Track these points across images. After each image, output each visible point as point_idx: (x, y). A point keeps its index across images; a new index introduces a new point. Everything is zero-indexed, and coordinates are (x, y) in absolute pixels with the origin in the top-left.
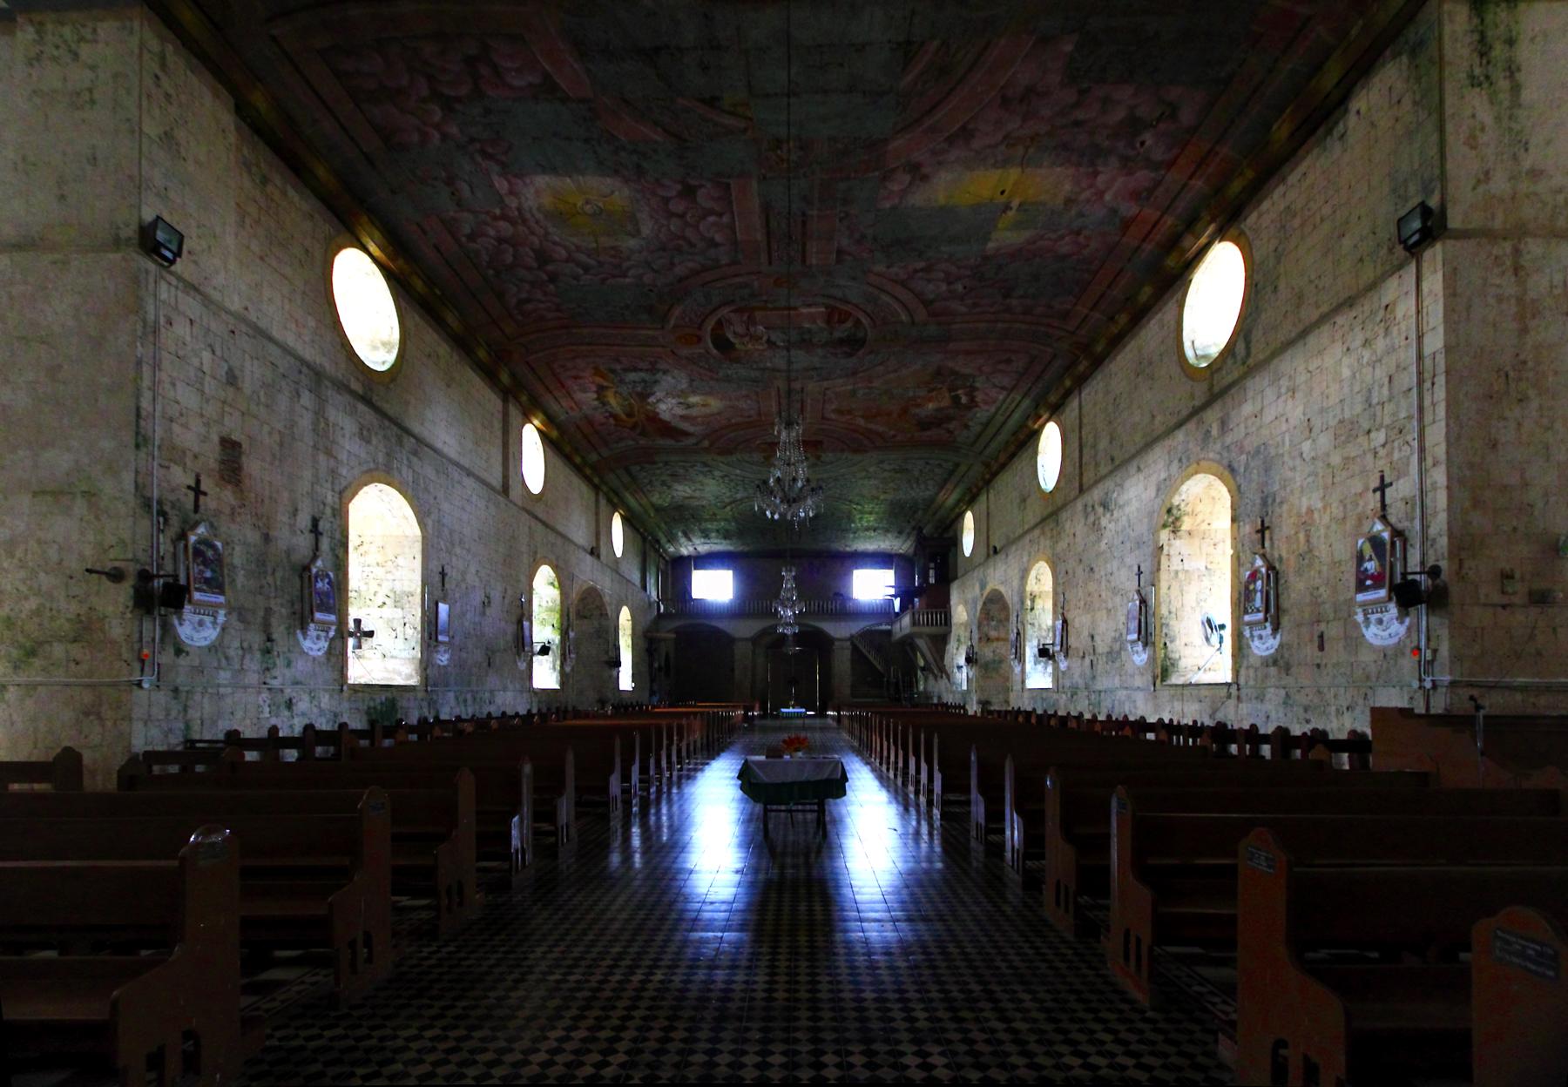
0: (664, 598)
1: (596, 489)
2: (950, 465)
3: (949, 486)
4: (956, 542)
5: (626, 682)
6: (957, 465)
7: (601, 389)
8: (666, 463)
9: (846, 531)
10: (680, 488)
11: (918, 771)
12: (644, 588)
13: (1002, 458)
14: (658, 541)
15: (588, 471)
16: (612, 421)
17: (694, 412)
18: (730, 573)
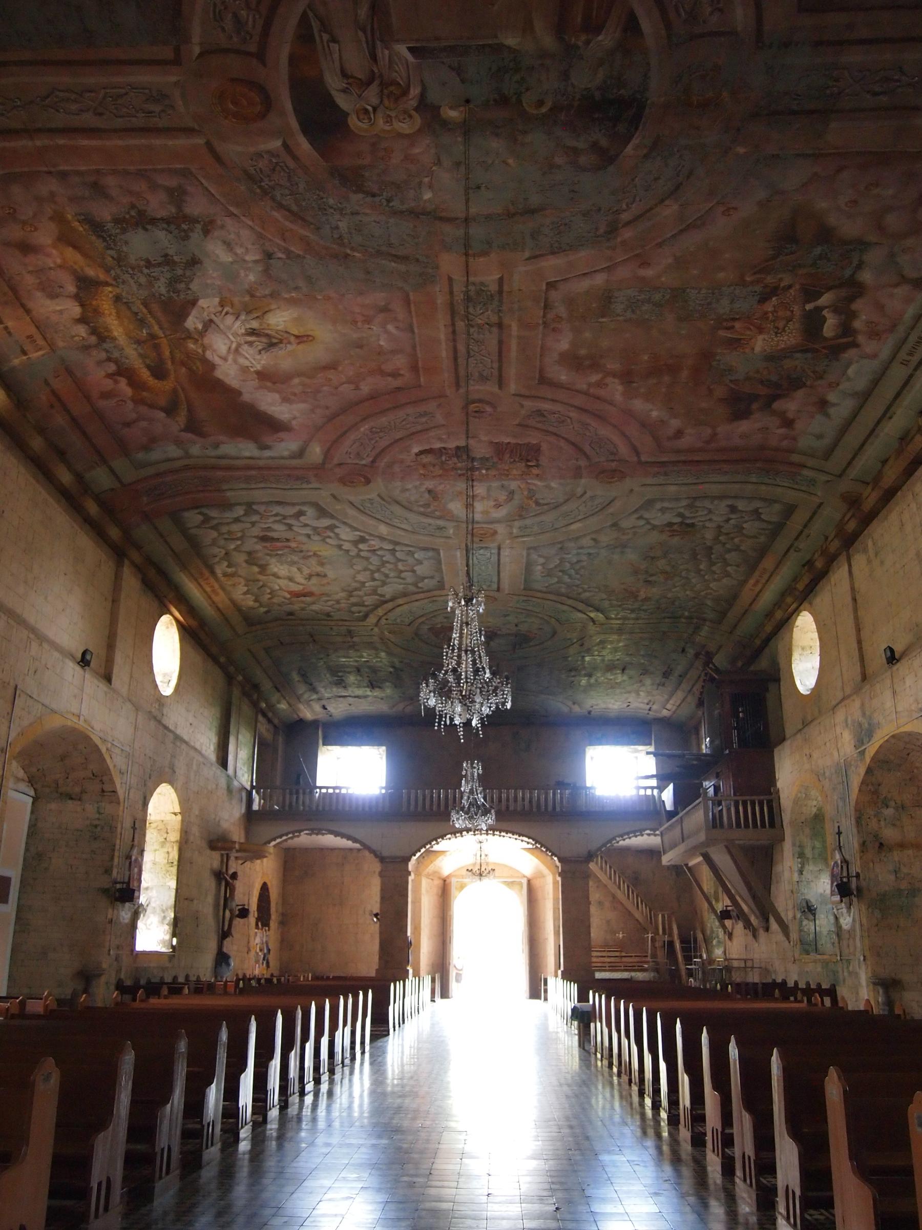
0: (263, 780)
1: (119, 553)
2: (772, 514)
3: (768, 563)
4: (777, 675)
5: (152, 935)
6: (790, 510)
7: (86, 287)
8: (250, 508)
9: (573, 670)
10: (282, 570)
11: (727, 1118)
12: (223, 762)
13: (890, 475)
14: (256, 687)
15: (92, 508)
16: (123, 385)
17: (284, 359)
18: (384, 748)
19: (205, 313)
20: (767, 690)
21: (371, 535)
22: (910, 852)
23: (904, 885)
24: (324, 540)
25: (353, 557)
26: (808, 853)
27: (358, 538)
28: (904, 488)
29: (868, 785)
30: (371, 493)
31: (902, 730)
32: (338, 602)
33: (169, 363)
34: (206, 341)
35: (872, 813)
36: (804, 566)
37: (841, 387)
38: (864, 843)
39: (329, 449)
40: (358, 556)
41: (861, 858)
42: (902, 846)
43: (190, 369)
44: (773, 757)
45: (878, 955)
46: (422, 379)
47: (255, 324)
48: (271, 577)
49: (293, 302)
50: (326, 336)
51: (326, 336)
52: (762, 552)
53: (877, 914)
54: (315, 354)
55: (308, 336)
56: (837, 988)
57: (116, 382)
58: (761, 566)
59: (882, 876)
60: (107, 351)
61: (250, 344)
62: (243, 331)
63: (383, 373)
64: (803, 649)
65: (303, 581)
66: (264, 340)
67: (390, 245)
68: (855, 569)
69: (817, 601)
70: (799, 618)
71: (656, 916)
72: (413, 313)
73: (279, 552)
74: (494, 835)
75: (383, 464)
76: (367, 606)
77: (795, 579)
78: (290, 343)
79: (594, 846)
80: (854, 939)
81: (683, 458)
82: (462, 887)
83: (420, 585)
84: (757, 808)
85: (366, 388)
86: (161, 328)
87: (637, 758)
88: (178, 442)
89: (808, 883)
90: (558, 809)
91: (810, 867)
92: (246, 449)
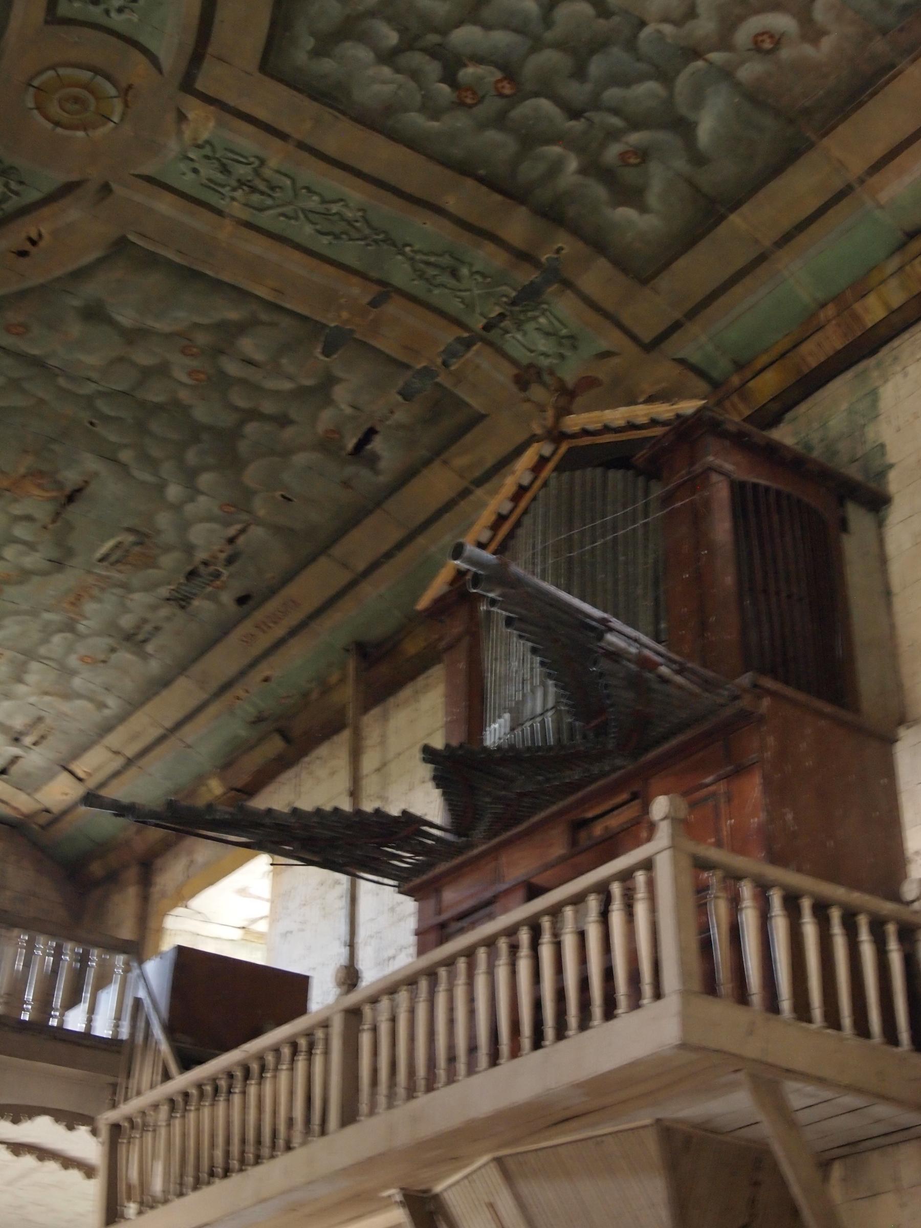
44: (889, 770)
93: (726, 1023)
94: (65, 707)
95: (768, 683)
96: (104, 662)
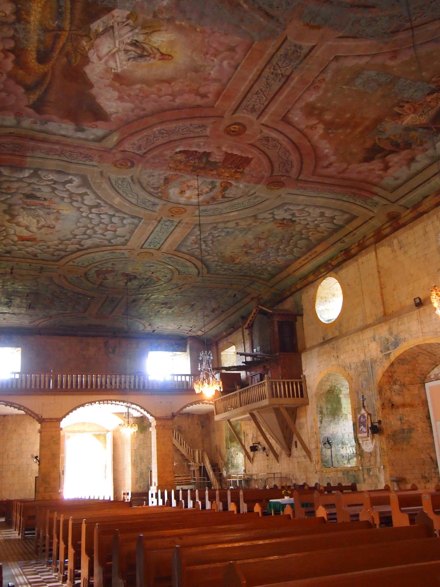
2: (339, 220)
3: (319, 249)
18: (20, 349)
19: (112, 21)
20: (296, 320)
21: (106, 203)
22: (408, 409)
23: (405, 427)
24: (71, 203)
25: (83, 217)
26: (325, 411)
27: (96, 204)
28: (431, 213)
29: (388, 372)
30: (127, 174)
31: (427, 342)
32: (49, 247)
33: (57, 52)
34: (98, 41)
35: (388, 388)
36: (341, 251)
37: (427, 152)
38: (383, 404)
39: (123, 140)
40: (87, 217)
41: (382, 412)
42: (404, 405)
43: (69, 62)
44: (300, 359)
45: (393, 465)
46: (217, 103)
47: (141, 38)
48: (14, 225)
49: (180, 29)
50: (182, 56)
51: (182, 56)
52: (320, 241)
53: (392, 443)
54: (166, 69)
55: (169, 55)
56: (357, 485)
57: (6, 57)
58: (315, 250)
59: (393, 422)
60: (16, 30)
61: (126, 51)
62: (129, 41)
63: (198, 94)
64: (322, 298)
65: (34, 229)
66: (139, 51)
67: (271, 6)
68: (379, 255)
69: (343, 272)
70: (324, 281)
71: (194, 452)
72: (246, 57)
73: (33, 207)
74: (108, 403)
75: (150, 156)
76: (67, 252)
77: (332, 259)
78: (154, 58)
79: (175, 410)
80: (375, 457)
81: (320, 180)
82: (69, 437)
83: (112, 241)
84: (294, 386)
85: (178, 101)
86: (71, 23)
87: (173, 359)
88: (19, 115)
89: (325, 428)
90: (137, 387)
91: (326, 419)
92: (65, 128)
93: (276, 401)
94: (198, 323)
95: (281, 353)
96: (370, 25)
